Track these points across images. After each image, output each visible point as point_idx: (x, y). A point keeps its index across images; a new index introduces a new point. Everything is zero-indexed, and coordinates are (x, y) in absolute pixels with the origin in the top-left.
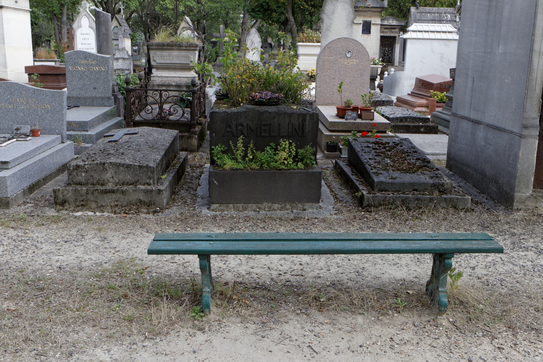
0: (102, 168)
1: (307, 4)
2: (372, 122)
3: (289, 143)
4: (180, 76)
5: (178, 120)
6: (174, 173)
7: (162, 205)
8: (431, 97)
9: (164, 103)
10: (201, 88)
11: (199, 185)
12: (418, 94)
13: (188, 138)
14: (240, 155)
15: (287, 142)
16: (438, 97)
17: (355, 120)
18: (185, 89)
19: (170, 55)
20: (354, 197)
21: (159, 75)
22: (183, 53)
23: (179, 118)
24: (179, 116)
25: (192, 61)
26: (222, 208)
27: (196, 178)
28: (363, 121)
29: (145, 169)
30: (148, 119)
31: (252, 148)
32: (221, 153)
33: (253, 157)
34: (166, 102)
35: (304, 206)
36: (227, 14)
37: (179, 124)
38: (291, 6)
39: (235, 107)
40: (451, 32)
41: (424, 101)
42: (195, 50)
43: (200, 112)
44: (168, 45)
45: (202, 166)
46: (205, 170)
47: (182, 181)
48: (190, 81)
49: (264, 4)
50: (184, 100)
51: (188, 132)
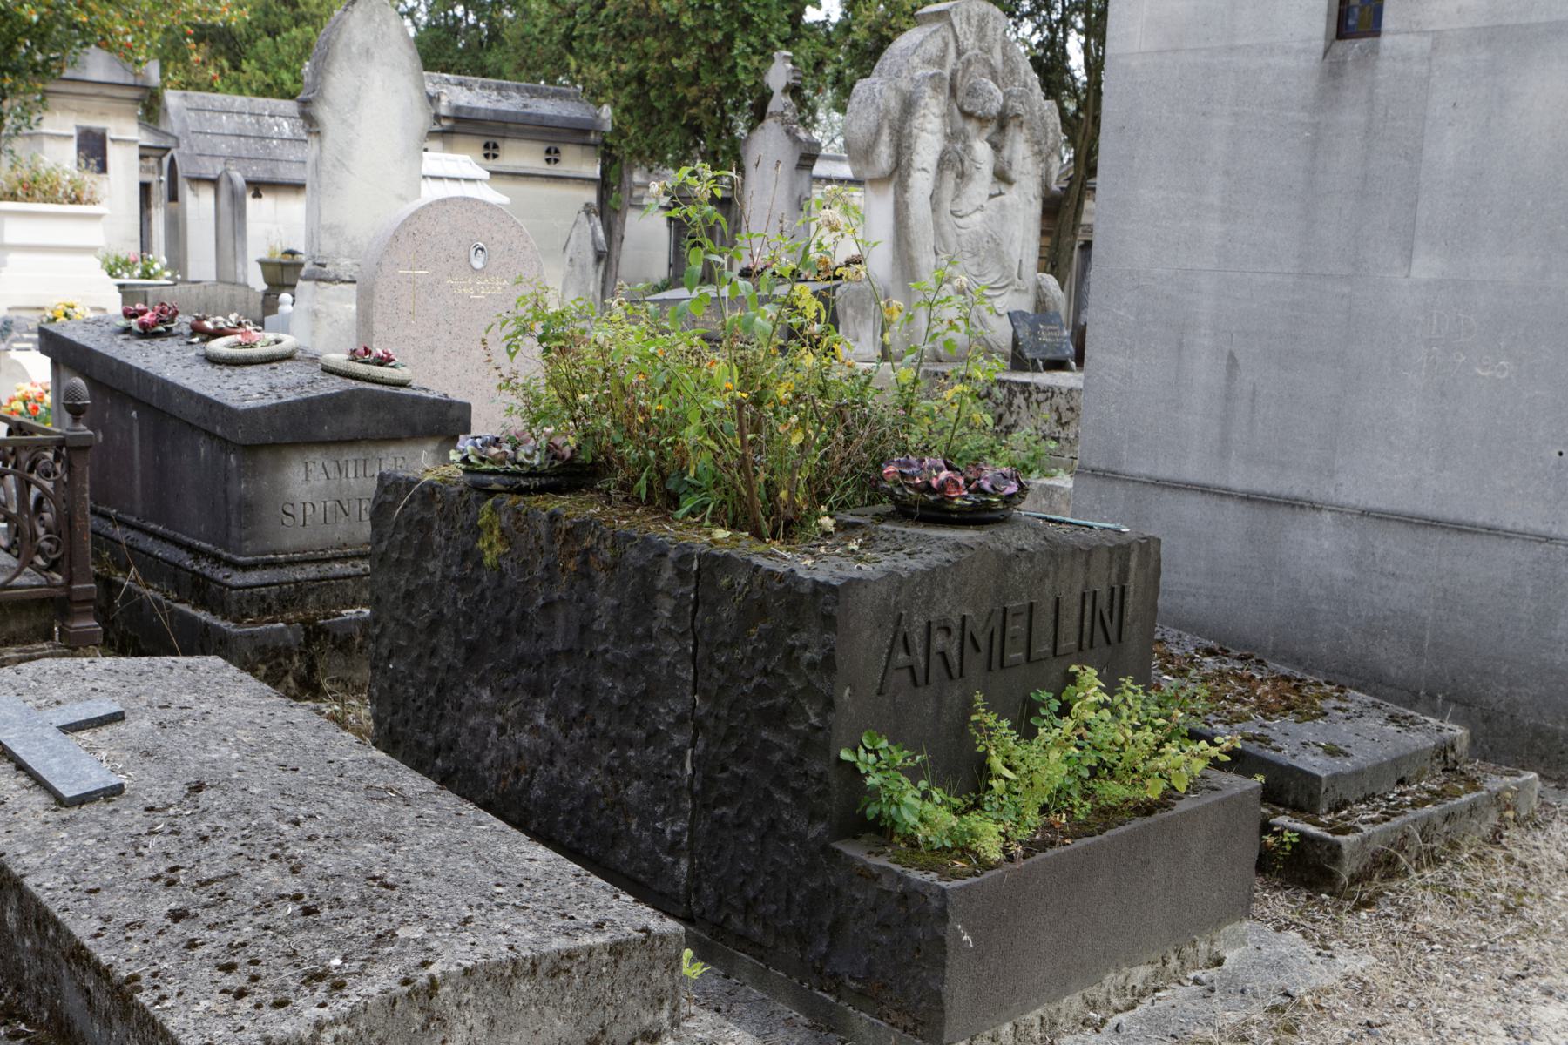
0: (418, 1018)
29: (638, 958)
40: (473, 180)
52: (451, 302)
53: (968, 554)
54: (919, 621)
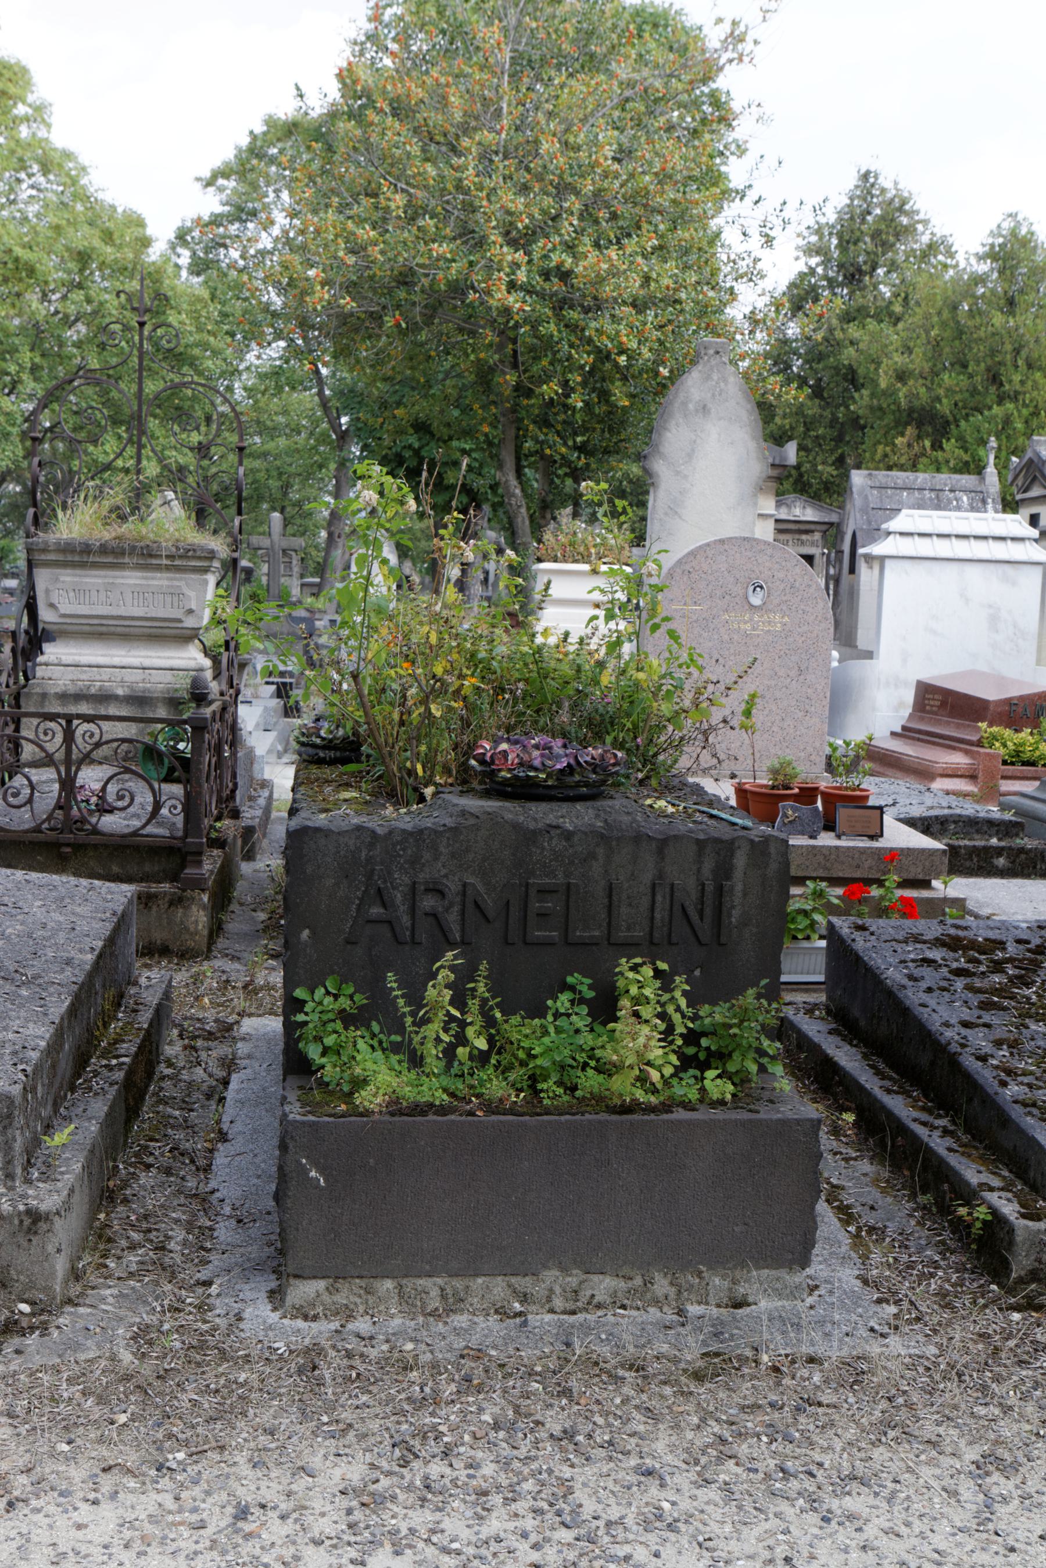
1: (565, 444)
2: (875, 844)
3: (658, 974)
4: (147, 663)
5: (135, 834)
6: (113, 1091)
7: (47, 1289)
8: (979, 744)
9: (80, 763)
10: (224, 709)
11: (223, 1137)
12: (920, 732)
13: (171, 904)
14: (438, 1040)
15: (648, 971)
16: (1005, 745)
17: (813, 837)
18: (162, 712)
19: (109, 588)
20: (960, 1227)
21: (67, 659)
22: (160, 580)
23: (137, 823)
24: (136, 816)
25: (190, 611)
26: (341, 1299)
27: (209, 1097)
28: (843, 843)
30: (14, 827)
31: (484, 1001)
32: (339, 1026)
33: (491, 1040)
34: (87, 759)
35: (735, 1282)
36: (286, 487)
37: (137, 848)
38: (511, 447)
39: (397, 804)
40: (1022, 539)
41: (958, 759)
42: (206, 570)
43: (219, 801)
44: (104, 549)
45: (229, 1028)
46: (242, 1048)
47: (147, 1113)
48: (183, 683)
49: (407, 454)
50: (160, 755)
51: (174, 878)
52: (726, 637)
53: (472, 821)
54: (401, 878)
